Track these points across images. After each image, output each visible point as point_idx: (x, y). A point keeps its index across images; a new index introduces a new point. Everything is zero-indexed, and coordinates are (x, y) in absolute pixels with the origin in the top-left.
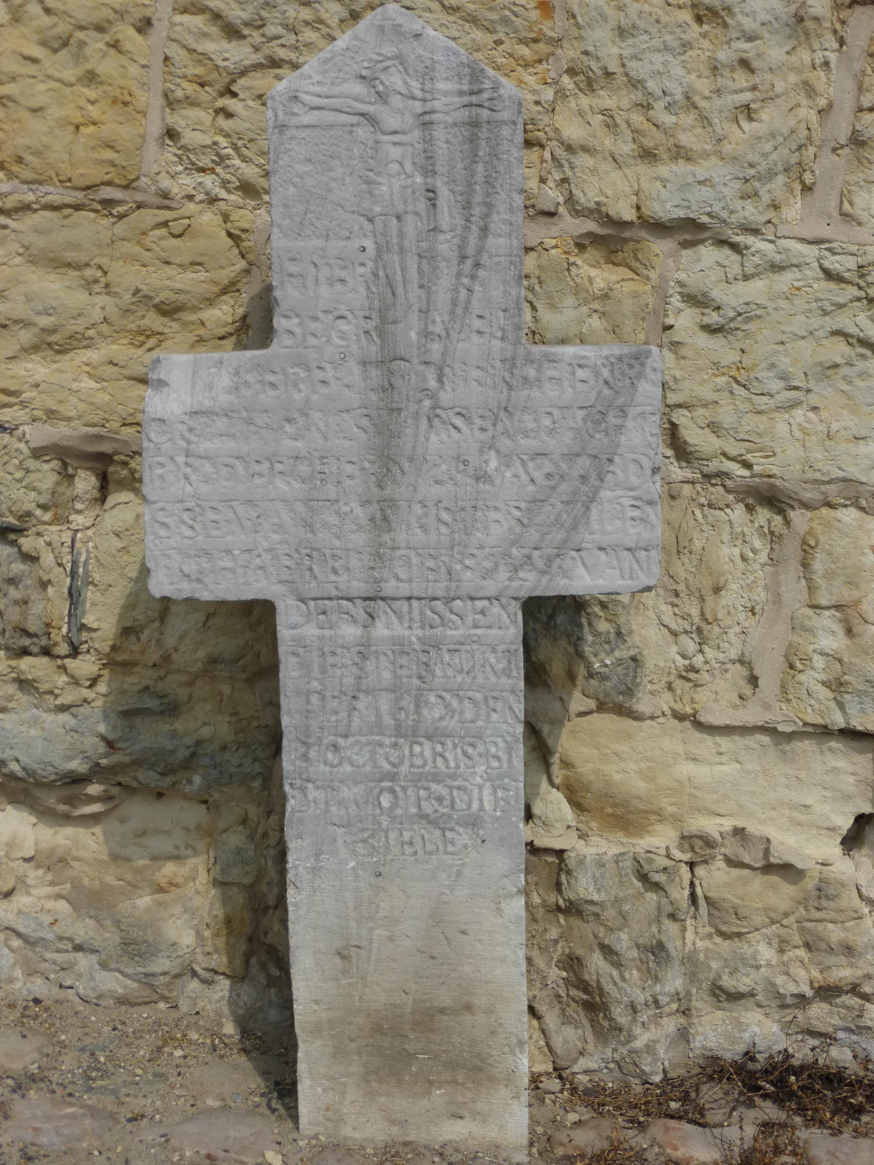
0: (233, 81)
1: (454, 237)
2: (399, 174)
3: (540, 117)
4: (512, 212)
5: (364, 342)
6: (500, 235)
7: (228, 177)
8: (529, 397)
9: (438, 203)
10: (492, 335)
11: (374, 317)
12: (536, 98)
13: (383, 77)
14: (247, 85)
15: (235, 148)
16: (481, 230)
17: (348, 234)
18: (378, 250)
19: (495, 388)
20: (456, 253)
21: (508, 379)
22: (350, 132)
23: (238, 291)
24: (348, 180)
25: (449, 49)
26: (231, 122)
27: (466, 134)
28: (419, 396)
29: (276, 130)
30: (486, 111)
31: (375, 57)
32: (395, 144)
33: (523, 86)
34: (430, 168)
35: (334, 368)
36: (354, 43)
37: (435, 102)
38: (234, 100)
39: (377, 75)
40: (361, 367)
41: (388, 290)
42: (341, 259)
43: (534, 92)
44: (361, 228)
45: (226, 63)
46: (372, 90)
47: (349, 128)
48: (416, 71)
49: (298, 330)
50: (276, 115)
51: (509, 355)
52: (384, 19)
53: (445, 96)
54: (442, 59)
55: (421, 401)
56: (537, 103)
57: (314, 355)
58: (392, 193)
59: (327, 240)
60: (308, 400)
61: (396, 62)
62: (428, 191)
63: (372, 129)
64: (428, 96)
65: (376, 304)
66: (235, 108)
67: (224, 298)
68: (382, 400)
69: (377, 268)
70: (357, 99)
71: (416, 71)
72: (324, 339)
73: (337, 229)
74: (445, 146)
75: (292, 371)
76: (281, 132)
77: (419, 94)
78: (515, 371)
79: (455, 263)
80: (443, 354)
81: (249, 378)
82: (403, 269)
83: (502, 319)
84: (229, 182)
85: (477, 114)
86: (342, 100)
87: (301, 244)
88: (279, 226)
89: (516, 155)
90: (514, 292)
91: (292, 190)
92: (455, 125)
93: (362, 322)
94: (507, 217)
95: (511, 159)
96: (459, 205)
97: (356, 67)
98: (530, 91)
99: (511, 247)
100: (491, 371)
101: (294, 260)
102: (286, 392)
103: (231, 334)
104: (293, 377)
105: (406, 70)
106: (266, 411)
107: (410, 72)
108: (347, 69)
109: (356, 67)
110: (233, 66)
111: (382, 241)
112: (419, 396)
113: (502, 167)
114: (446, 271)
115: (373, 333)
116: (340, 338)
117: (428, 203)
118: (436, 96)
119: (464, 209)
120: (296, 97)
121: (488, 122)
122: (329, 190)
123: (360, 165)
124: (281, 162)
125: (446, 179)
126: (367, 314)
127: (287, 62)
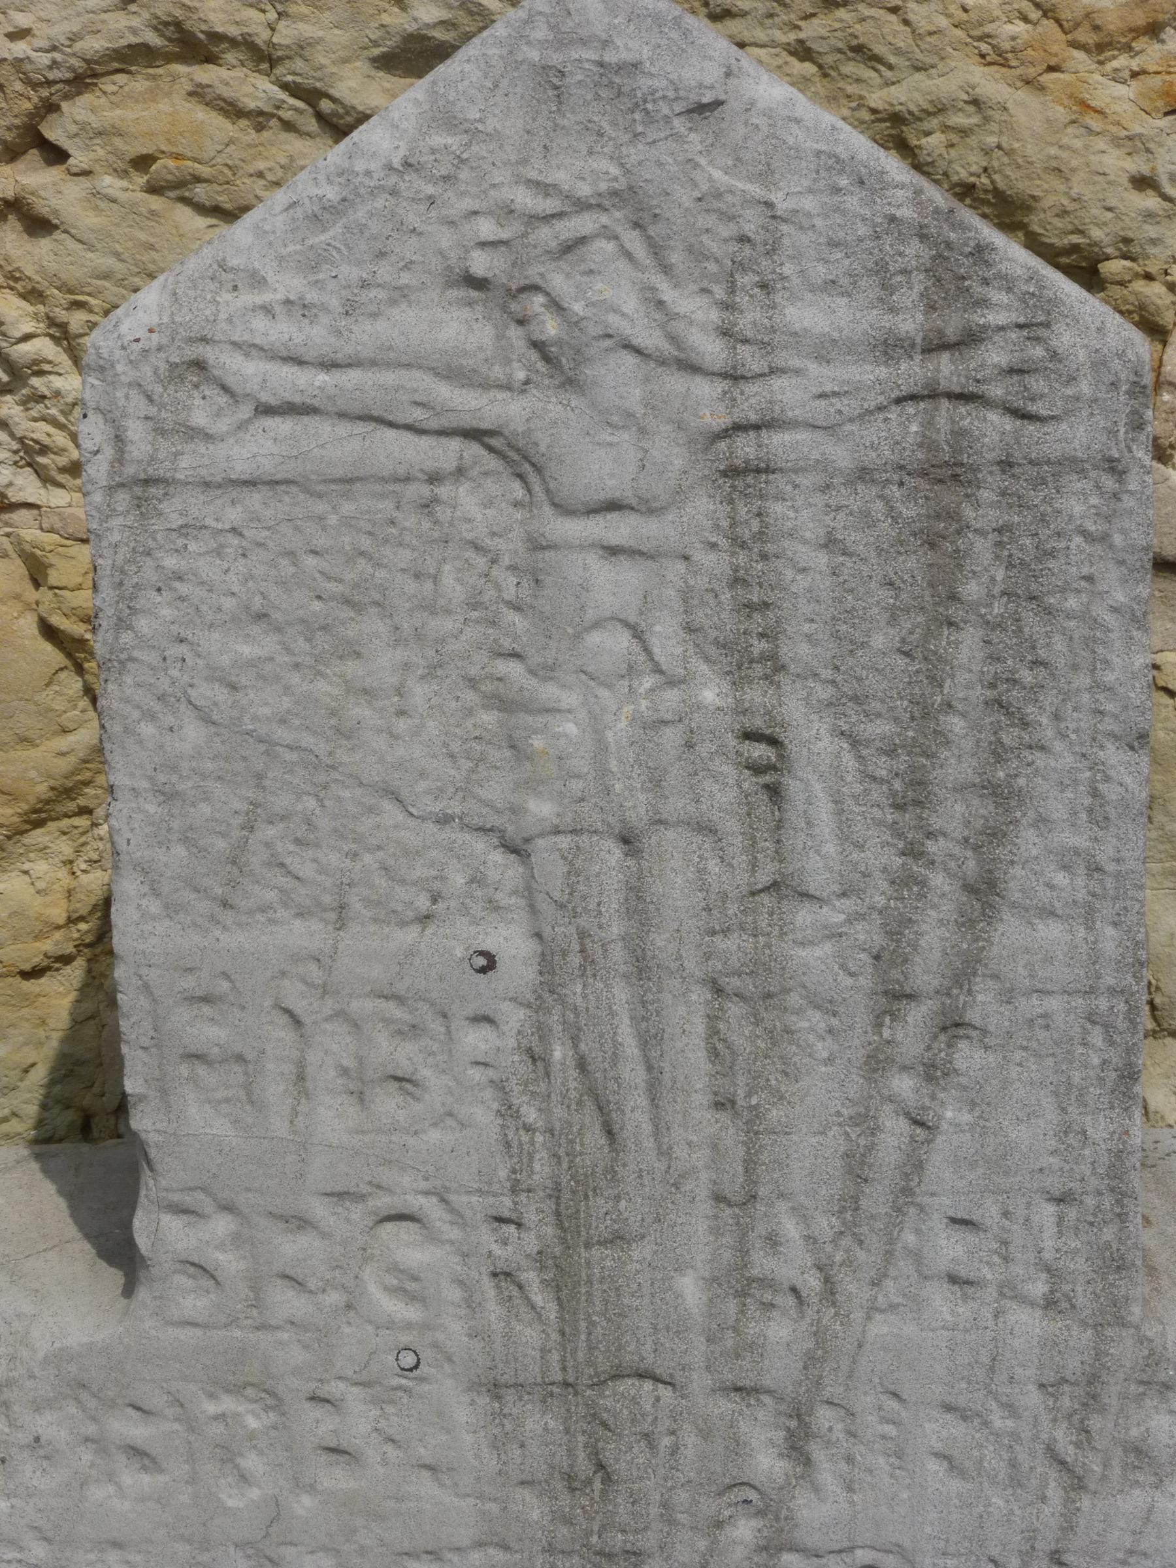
0: (50, 108)
1: (855, 917)
2: (632, 671)
3: (1152, 231)
4: (1099, 818)
5: (494, 1311)
6: (1049, 913)
7: (41, 431)
8: (1148, 1515)
9: (793, 787)
10: (1009, 1291)
11: (531, 1217)
12: (1138, 165)
13: (558, 282)
14: (95, 122)
15: (62, 335)
16: (969, 889)
17: (423, 903)
18: (547, 962)
19: (1016, 1481)
20: (865, 982)
21: (1069, 1452)
22: (428, 506)
23: (86, 811)
24: (419, 693)
25: (839, 164)
26: (44, 246)
27: (909, 511)
28: (709, 1507)
29: (123, 499)
30: (994, 417)
31: (525, 199)
32: (612, 551)
33: (1095, 123)
34: (760, 647)
35: (376, 1401)
36: (438, 140)
37: (777, 383)
38: (55, 174)
39: (533, 273)
40: (483, 1400)
41: (589, 1115)
42: (399, 999)
43: (1133, 143)
44: (477, 880)
45: (20, 48)
46: (515, 333)
47: (419, 490)
48: (697, 254)
49: (229, 1262)
50: (119, 440)
51: (1073, 1365)
52: (561, 41)
53: (823, 359)
54: (809, 204)
55: (719, 1524)
56: (1143, 183)
57: (298, 1356)
58: (601, 747)
59: (341, 924)
60: (276, 1513)
61: (615, 219)
62: (749, 736)
63: (518, 491)
64: (751, 359)
65: (542, 1168)
66: (54, 202)
67: (38, 836)
68: (568, 1521)
69: (543, 1033)
70: (453, 374)
71: (697, 254)
72: (334, 1298)
73: (381, 881)
74: (822, 560)
75: (211, 1408)
76: (139, 503)
77: (711, 350)
78: (1095, 1422)
79: (863, 1019)
80: (811, 1360)
81: (47, 1425)
82: (650, 1040)
83: (1050, 1230)
84: (44, 450)
85: (959, 433)
86: (389, 378)
87: (235, 939)
88: (143, 869)
89: (1120, 597)
90: (1099, 1129)
91: (193, 732)
92: (863, 474)
93: (486, 1238)
94: (1081, 841)
95: (1101, 612)
96: (877, 793)
97: (445, 239)
98: (1116, 142)
99: (1095, 957)
100: (999, 1421)
101: (206, 999)
102: (193, 1480)
103: (66, 960)
104: (218, 1429)
105: (656, 250)
106: (117, 1545)
107: (676, 258)
108: (409, 248)
109: (445, 239)
110: (44, 59)
111: (563, 932)
112: (709, 1507)
113: (1059, 644)
114: (822, 1049)
115: (530, 1277)
116: (399, 1291)
117: (750, 782)
118: (783, 358)
119: (899, 807)
120: (199, 365)
121: (1006, 464)
122: (345, 733)
123: (471, 634)
124: (143, 624)
125: (824, 693)
126: (505, 1205)
127: (233, 43)
